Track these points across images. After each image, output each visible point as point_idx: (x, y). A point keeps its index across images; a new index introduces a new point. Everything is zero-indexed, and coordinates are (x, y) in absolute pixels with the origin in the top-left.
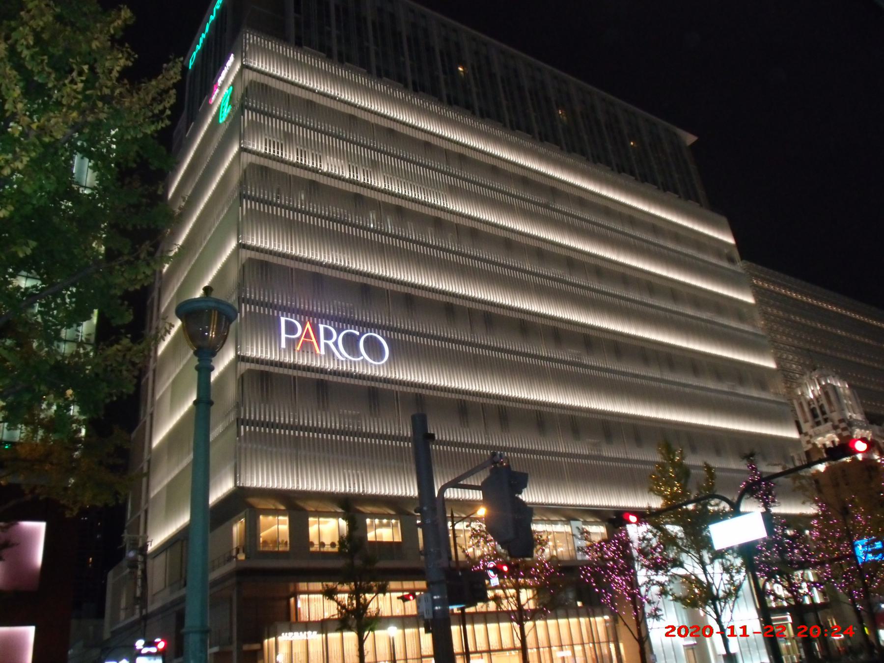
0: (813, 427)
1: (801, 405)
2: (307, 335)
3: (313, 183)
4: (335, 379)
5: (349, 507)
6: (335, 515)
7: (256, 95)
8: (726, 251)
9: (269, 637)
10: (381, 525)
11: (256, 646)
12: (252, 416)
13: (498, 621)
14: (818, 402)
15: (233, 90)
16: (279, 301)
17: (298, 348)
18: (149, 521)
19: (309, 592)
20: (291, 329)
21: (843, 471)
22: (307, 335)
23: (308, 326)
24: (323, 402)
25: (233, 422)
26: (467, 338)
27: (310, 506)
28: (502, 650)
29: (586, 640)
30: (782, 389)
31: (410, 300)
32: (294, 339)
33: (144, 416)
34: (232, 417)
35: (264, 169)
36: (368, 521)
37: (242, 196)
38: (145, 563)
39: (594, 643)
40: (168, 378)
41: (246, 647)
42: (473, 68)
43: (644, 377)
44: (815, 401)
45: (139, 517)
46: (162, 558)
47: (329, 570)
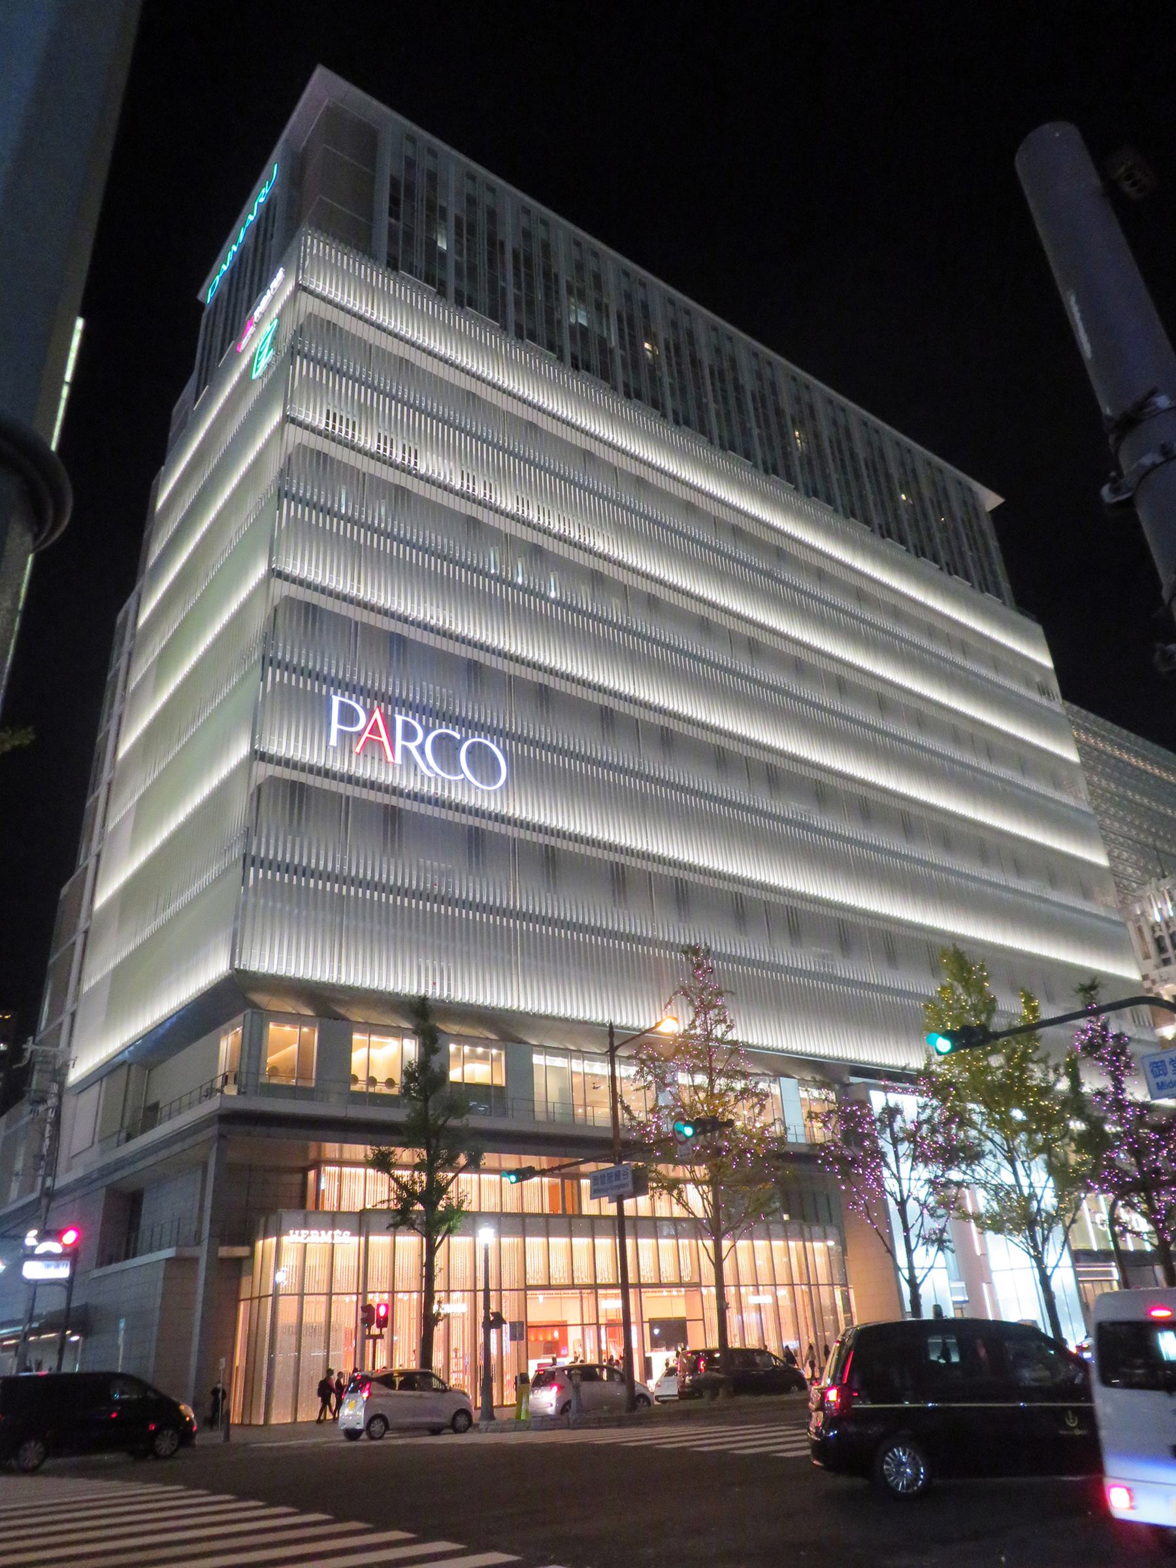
0: (1157, 967)
1: (1140, 930)
2: (375, 730)
3: (401, 492)
4: (415, 807)
5: (424, 1018)
6: (398, 1033)
7: (316, 343)
8: (1038, 679)
9: (265, 1236)
10: (475, 1057)
11: (241, 1251)
12: (271, 853)
13: (656, 1235)
14: (1168, 926)
15: (278, 326)
16: (331, 669)
17: (358, 750)
18: (76, 1032)
19: (341, 1163)
20: (348, 715)
21: (571, 1231)
22: (375, 730)
23: (377, 715)
24: (393, 841)
25: (236, 862)
26: (631, 763)
27: (357, 1015)
28: (659, 1285)
29: (796, 1280)
30: (1111, 899)
31: (545, 694)
32: (351, 733)
33: (86, 858)
34: (237, 852)
35: (322, 458)
36: (452, 1047)
37: (282, 494)
38: (60, 1097)
39: (809, 1284)
40: (132, 796)
41: (224, 1251)
42: (667, 348)
43: (906, 858)
44: (1164, 926)
45: (61, 1024)
46: (94, 1091)
47: (373, 1128)
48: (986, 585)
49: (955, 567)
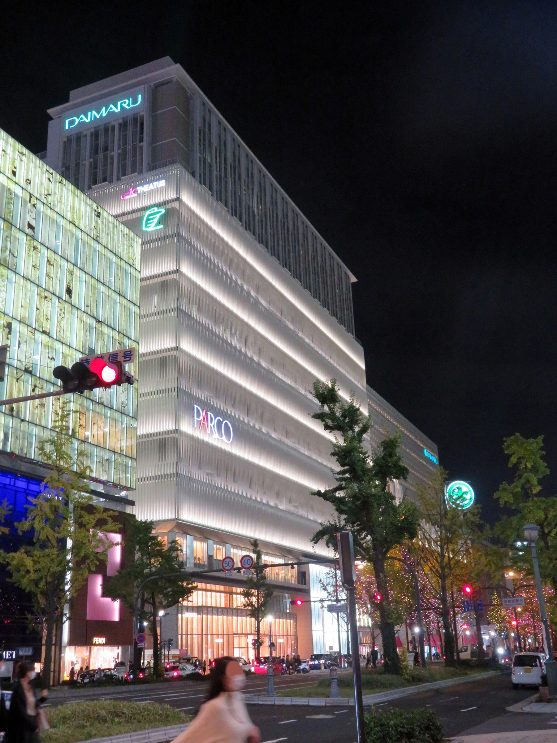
48: (342, 321)
49: (204, 179)
